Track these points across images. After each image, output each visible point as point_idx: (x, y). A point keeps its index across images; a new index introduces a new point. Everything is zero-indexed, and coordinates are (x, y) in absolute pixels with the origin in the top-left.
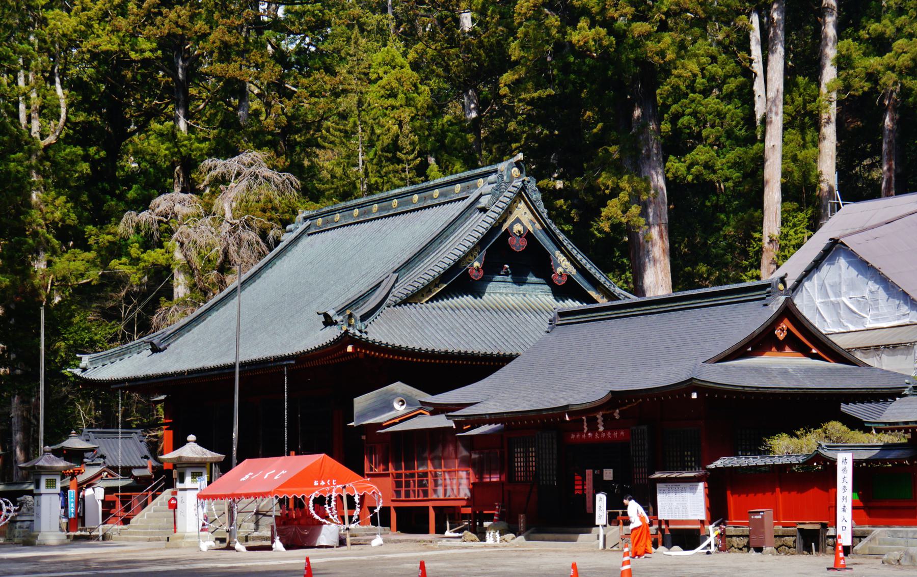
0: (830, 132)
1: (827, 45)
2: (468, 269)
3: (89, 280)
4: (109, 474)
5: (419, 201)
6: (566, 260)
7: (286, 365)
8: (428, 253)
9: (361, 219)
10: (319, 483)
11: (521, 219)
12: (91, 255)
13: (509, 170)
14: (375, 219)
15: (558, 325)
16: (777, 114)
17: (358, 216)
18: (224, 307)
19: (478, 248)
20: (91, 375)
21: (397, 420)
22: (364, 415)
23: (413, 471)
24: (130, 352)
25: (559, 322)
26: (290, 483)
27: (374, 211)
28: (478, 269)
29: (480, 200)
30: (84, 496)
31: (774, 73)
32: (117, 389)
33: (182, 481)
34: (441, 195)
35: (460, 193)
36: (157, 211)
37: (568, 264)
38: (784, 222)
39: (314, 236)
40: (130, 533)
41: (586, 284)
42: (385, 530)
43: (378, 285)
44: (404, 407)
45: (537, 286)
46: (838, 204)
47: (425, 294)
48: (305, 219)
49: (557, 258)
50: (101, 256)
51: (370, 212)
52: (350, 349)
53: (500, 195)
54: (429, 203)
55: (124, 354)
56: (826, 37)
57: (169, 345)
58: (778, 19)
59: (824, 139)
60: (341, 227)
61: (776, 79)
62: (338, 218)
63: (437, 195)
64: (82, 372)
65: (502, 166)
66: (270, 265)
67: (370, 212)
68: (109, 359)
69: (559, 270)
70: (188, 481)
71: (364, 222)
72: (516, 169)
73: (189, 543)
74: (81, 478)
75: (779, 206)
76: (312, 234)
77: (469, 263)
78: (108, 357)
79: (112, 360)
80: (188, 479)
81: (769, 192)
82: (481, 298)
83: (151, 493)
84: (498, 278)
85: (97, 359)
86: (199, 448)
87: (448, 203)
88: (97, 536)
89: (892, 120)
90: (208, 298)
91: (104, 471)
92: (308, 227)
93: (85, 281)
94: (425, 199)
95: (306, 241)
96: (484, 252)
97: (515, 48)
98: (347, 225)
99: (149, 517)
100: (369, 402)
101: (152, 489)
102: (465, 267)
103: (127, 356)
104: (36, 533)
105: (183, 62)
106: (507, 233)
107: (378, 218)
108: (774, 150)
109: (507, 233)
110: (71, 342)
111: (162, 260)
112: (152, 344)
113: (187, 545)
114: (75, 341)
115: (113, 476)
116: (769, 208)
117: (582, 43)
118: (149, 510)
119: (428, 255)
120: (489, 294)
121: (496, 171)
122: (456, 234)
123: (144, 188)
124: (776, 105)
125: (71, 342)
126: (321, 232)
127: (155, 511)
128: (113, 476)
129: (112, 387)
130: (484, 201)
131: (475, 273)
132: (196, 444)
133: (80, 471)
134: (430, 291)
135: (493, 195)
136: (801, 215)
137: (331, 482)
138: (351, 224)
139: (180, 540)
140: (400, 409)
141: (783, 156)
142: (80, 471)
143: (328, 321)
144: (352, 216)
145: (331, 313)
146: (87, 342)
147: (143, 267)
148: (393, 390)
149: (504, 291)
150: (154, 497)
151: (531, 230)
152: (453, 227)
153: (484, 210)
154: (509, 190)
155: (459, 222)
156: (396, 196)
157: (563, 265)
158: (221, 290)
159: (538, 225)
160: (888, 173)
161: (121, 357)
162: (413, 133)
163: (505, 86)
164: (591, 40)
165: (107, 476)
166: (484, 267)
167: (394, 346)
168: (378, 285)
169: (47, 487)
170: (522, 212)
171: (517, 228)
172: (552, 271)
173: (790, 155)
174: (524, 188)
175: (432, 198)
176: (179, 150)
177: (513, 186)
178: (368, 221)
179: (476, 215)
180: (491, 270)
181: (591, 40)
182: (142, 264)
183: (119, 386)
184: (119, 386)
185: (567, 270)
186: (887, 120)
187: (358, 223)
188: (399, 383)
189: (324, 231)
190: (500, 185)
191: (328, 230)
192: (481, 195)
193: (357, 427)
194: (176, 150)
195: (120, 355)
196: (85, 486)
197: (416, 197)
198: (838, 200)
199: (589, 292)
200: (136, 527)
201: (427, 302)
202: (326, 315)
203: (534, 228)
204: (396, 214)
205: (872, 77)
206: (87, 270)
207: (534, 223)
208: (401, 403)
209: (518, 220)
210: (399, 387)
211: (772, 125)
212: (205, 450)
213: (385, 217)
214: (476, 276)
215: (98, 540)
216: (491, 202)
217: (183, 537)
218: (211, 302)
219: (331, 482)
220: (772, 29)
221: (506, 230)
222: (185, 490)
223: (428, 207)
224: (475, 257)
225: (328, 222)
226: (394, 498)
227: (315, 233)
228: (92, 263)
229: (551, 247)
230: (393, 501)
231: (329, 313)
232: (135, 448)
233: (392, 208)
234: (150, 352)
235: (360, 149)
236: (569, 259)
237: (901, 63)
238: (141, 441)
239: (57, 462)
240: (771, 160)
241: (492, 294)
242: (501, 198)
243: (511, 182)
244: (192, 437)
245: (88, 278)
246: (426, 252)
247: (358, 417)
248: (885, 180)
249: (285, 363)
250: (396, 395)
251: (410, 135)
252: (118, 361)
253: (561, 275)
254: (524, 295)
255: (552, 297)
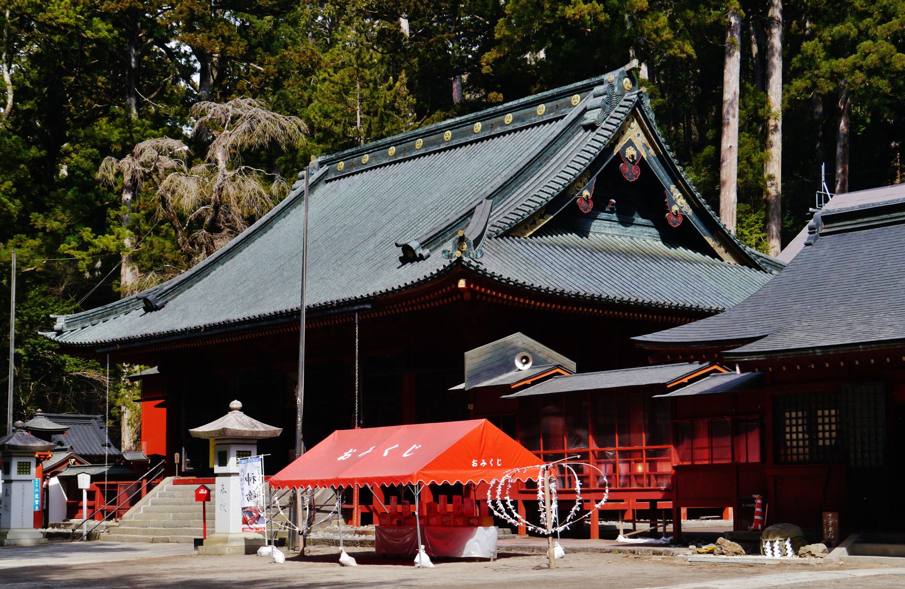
0: (776, 139)
1: (773, 55)
2: (576, 199)
3: (33, 269)
4: (77, 460)
5: (483, 129)
6: (682, 197)
7: (358, 311)
8: (526, 178)
9: (400, 158)
10: (479, 463)
11: (634, 141)
12: (36, 242)
13: (620, 80)
14: (419, 156)
15: (822, 235)
16: (734, 116)
17: (395, 155)
18: (231, 261)
19: (588, 173)
20: (69, 338)
21: (529, 382)
22: (477, 376)
23: (621, 448)
24: (116, 313)
25: (824, 231)
26: (439, 462)
27: (417, 147)
28: (587, 200)
29: (585, 116)
30: (47, 486)
31: (731, 75)
32: (105, 354)
33: (223, 462)
34: (515, 120)
35: (544, 114)
36: (142, 159)
37: (684, 201)
38: (739, 221)
39: (333, 183)
40: (124, 532)
41: (702, 228)
42: (505, 533)
43: (470, 213)
44: (530, 365)
45: (645, 229)
46: (826, 196)
47: (528, 226)
48: (321, 164)
49: (672, 194)
50: (46, 244)
51: (412, 148)
52: (462, 284)
53: (611, 110)
54: (499, 130)
55: (108, 315)
56: (772, 47)
57: (167, 302)
58: (735, 23)
59: (772, 146)
60: (371, 169)
61: (733, 82)
62: (367, 160)
63: (511, 120)
64: (57, 335)
65: (610, 77)
66: (283, 214)
67: (412, 148)
68: (91, 320)
69: (675, 208)
70: (233, 463)
71: (404, 160)
72: (627, 80)
73: (234, 548)
74: (47, 464)
75: (735, 206)
76: (331, 180)
77: (578, 191)
78: (90, 318)
79: (94, 322)
80: (232, 460)
81: (725, 192)
82: (587, 237)
83: (145, 483)
84: (603, 215)
85: (75, 320)
86: (246, 418)
87: (527, 128)
88: (81, 535)
89: (846, 124)
90: (193, 263)
91: (72, 458)
92: (326, 173)
93: (29, 269)
94: (492, 126)
95: (323, 189)
96: (594, 179)
97: (502, 26)
98: (380, 166)
99: (146, 511)
100: (483, 358)
101: (148, 478)
102: (573, 195)
103: (112, 317)
104: (6, 530)
105: (136, 50)
106: (619, 158)
107: (424, 155)
108: (730, 152)
109: (619, 158)
110: (26, 318)
111: (113, 247)
112: (146, 300)
113: (232, 551)
114: (30, 317)
115: (81, 463)
116: (726, 208)
117: (578, 17)
118: (146, 503)
119: (526, 179)
120: (594, 233)
121: (601, 83)
122: (558, 155)
123: (80, 191)
124: (733, 107)
125: (26, 318)
126: (344, 177)
127: (153, 504)
128: (81, 463)
129: (97, 351)
130: (590, 117)
131: (584, 204)
132: (242, 414)
133: (46, 456)
134: (534, 223)
135: (604, 109)
136: (753, 217)
137: (495, 462)
138: (385, 165)
139: (221, 545)
140: (524, 369)
141: (738, 158)
142: (46, 456)
143: (409, 256)
144: (387, 155)
145: (414, 245)
146: (43, 319)
147: (93, 253)
148: (512, 343)
149: (610, 232)
150: (150, 488)
151: (645, 156)
152: (554, 147)
153: (592, 127)
154: (620, 104)
155: (560, 142)
156: (449, 127)
157: (678, 202)
158: (209, 253)
159: (652, 151)
160: (842, 176)
161: (105, 319)
162: (412, 96)
163: (487, 65)
164: (586, 15)
165: (74, 463)
166: (595, 197)
167: (516, 283)
168: (470, 213)
169: (19, 472)
170: (634, 132)
171: (630, 152)
172: (665, 209)
173: (745, 157)
174: (639, 104)
175: (502, 124)
176: (131, 136)
177: (625, 100)
178: (409, 159)
179: (580, 134)
180: (599, 204)
181: (586, 15)
182: (91, 250)
183: (106, 349)
184: (106, 349)
185: (683, 210)
186: (842, 124)
187: (395, 163)
188: (519, 334)
189: (348, 175)
190: (610, 98)
191: (353, 174)
192: (585, 110)
193: (469, 391)
194: (128, 135)
195: (104, 317)
196: (49, 474)
197: (478, 126)
198: (825, 191)
199: (705, 238)
200: (131, 524)
201: (531, 237)
202: (406, 248)
203: (648, 154)
204: (450, 148)
205: (835, 76)
206: (32, 257)
207: (648, 149)
208: (524, 361)
209: (630, 143)
210: (518, 339)
211: (729, 127)
212: (254, 421)
213: (435, 152)
214: (586, 208)
215: (82, 540)
216: (601, 118)
217: (226, 541)
218: (195, 268)
219: (495, 462)
220: (729, 33)
221: (618, 153)
222: (228, 475)
223: (498, 135)
224: (585, 185)
225: (353, 165)
226: (525, 489)
227: (335, 179)
228: (38, 251)
229: (665, 180)
230: (521, 492)
231: (410, 244)
232: (94, 435)
233: (444, 141)
234: (142, 311)
235: (358, 107)
236: (685, 196)
237: (869, 62)
238: (101, 428)
239: (32, 441)
240: (728, 161)
241: (597, 235)
242: (612, 114)
243: (622, 95)
244: (236, 404)
245: (32, 266)
246: (524, 176)
247: (470, 378)
248: (839, 183)
249: (356, 308)
250: (516, 350)
251: (408, 98)
252: (101, 323)
253: (676, 215)
254: (632, 238)
255: (661, 243)
